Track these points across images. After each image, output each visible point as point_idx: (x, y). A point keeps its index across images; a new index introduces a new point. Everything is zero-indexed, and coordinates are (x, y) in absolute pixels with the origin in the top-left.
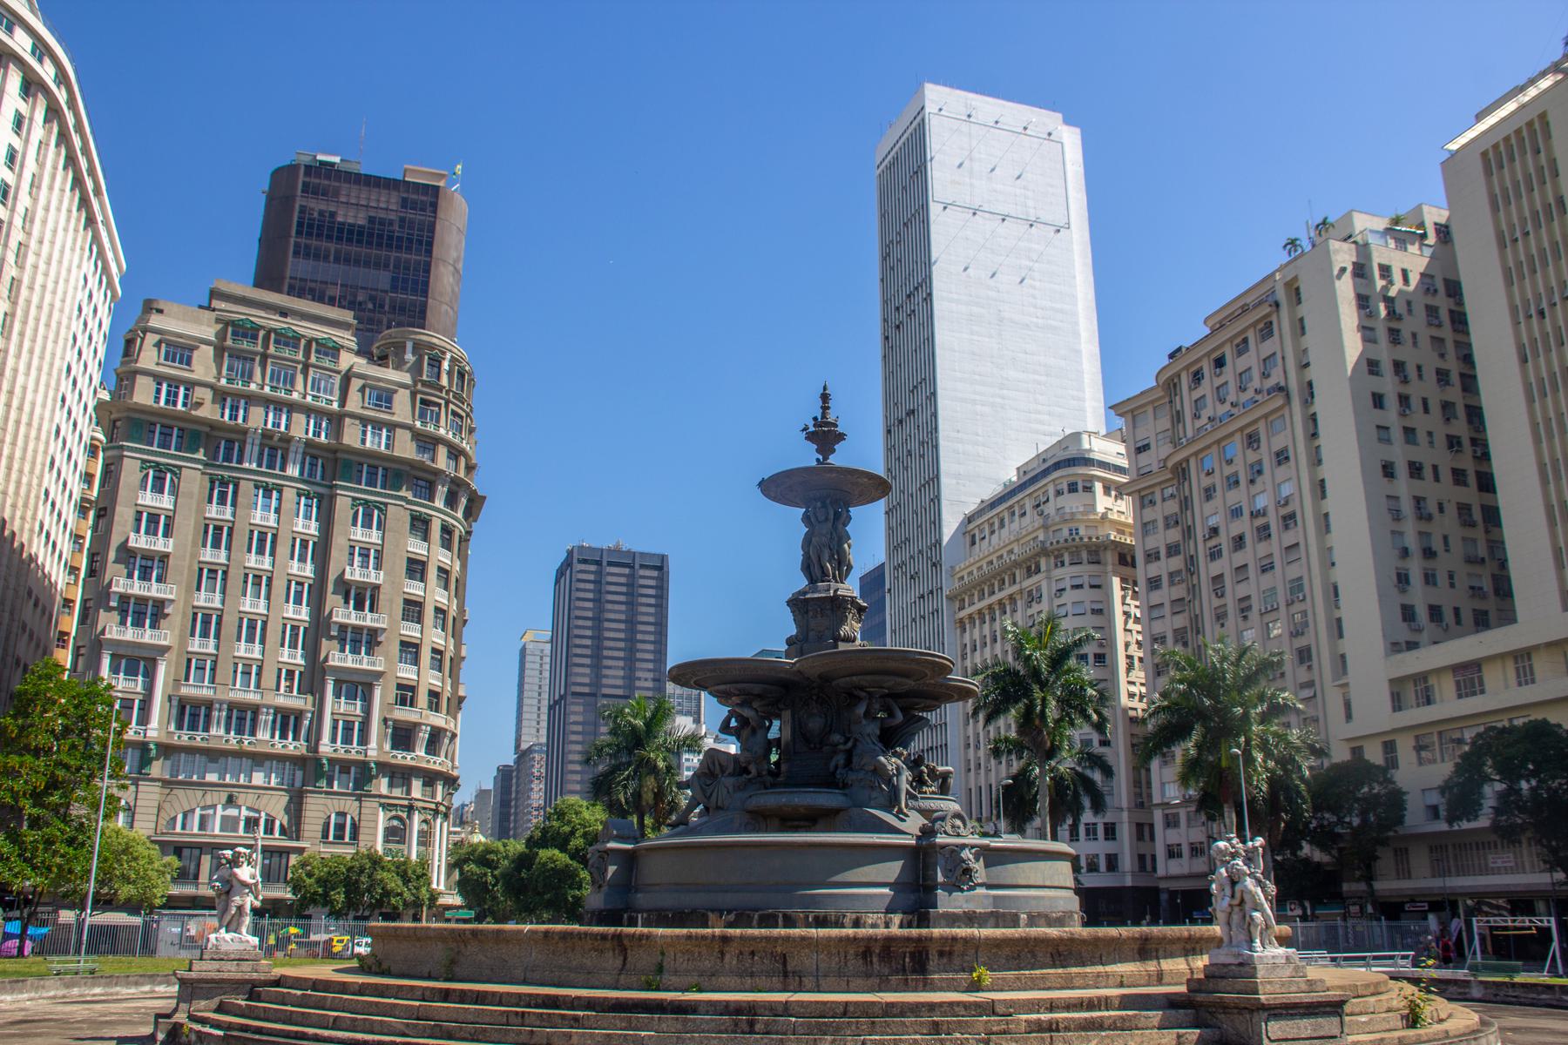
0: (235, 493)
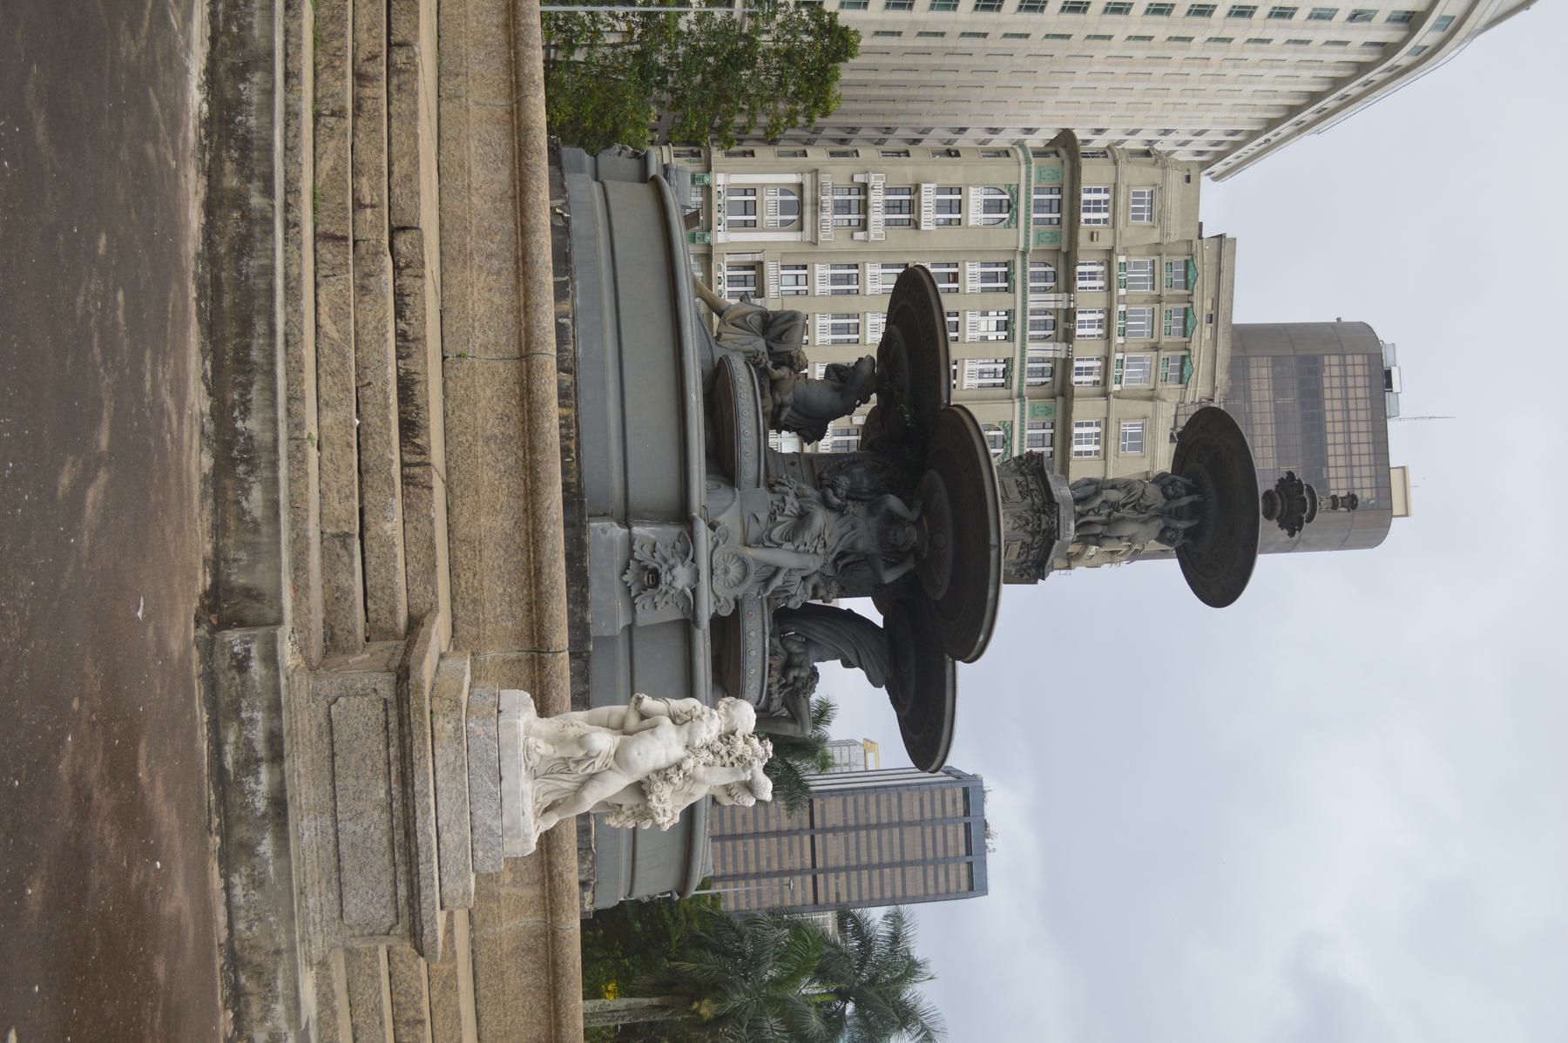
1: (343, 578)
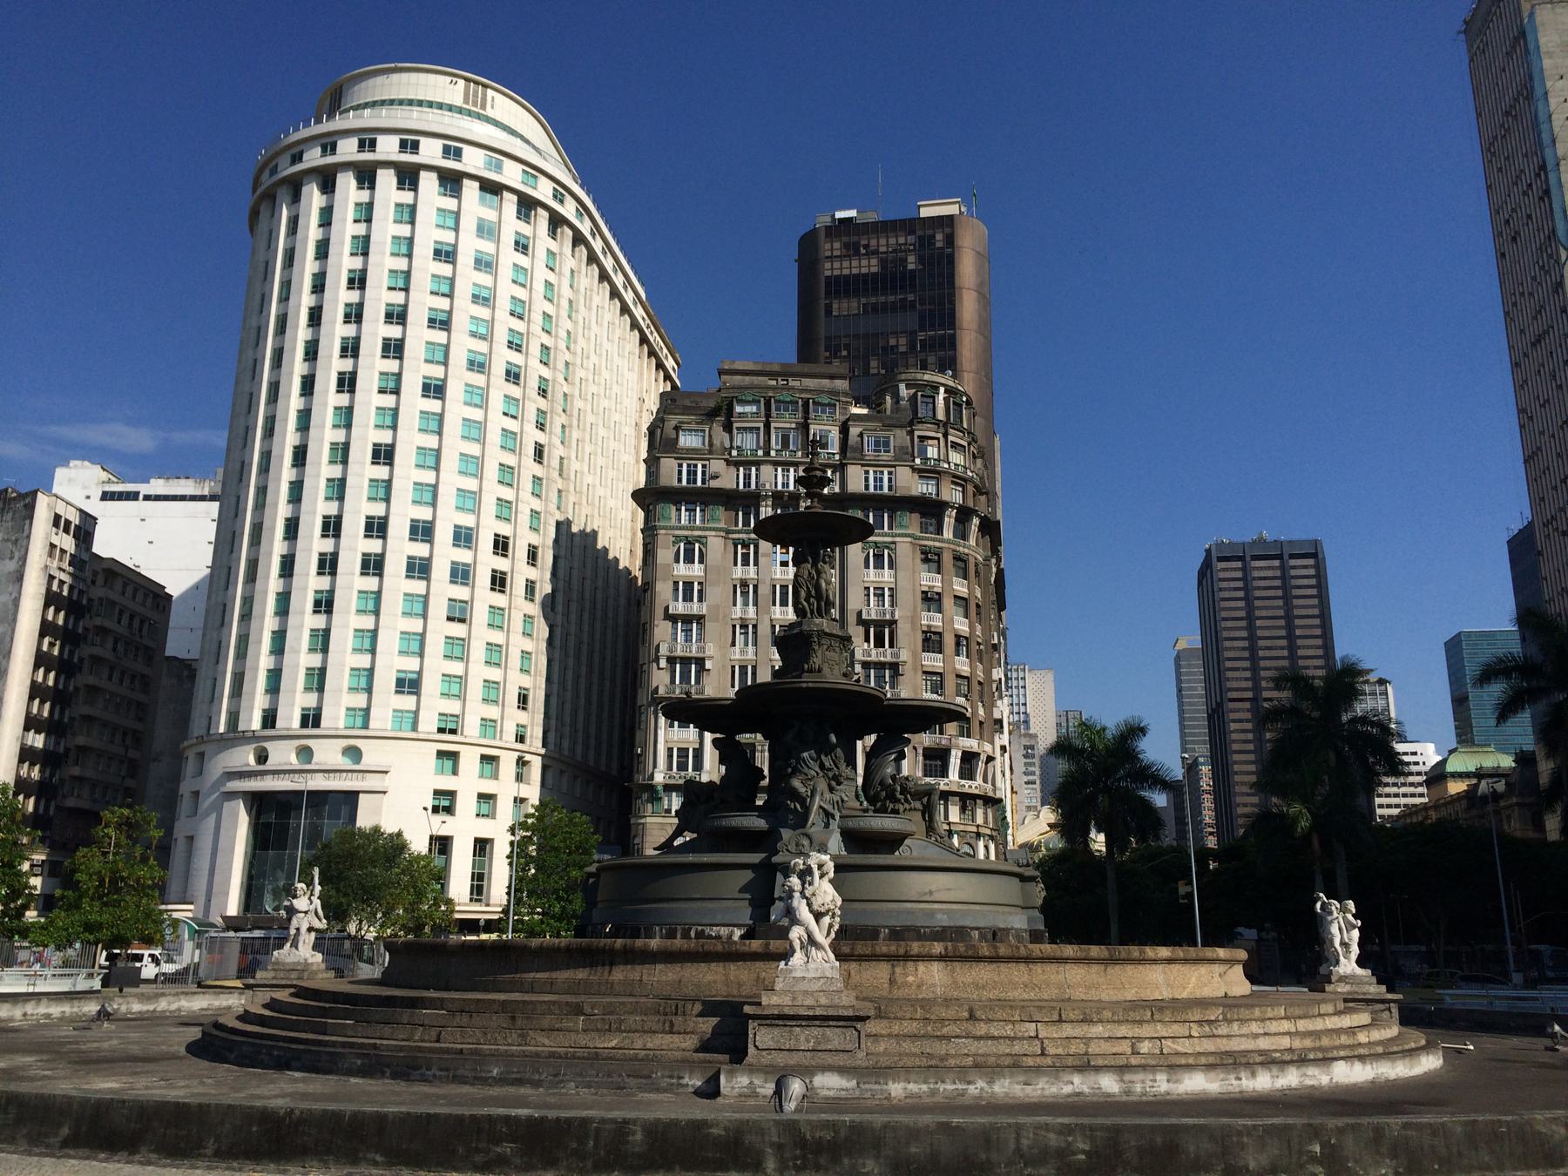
0: (756, 553)
1: (482, 923)
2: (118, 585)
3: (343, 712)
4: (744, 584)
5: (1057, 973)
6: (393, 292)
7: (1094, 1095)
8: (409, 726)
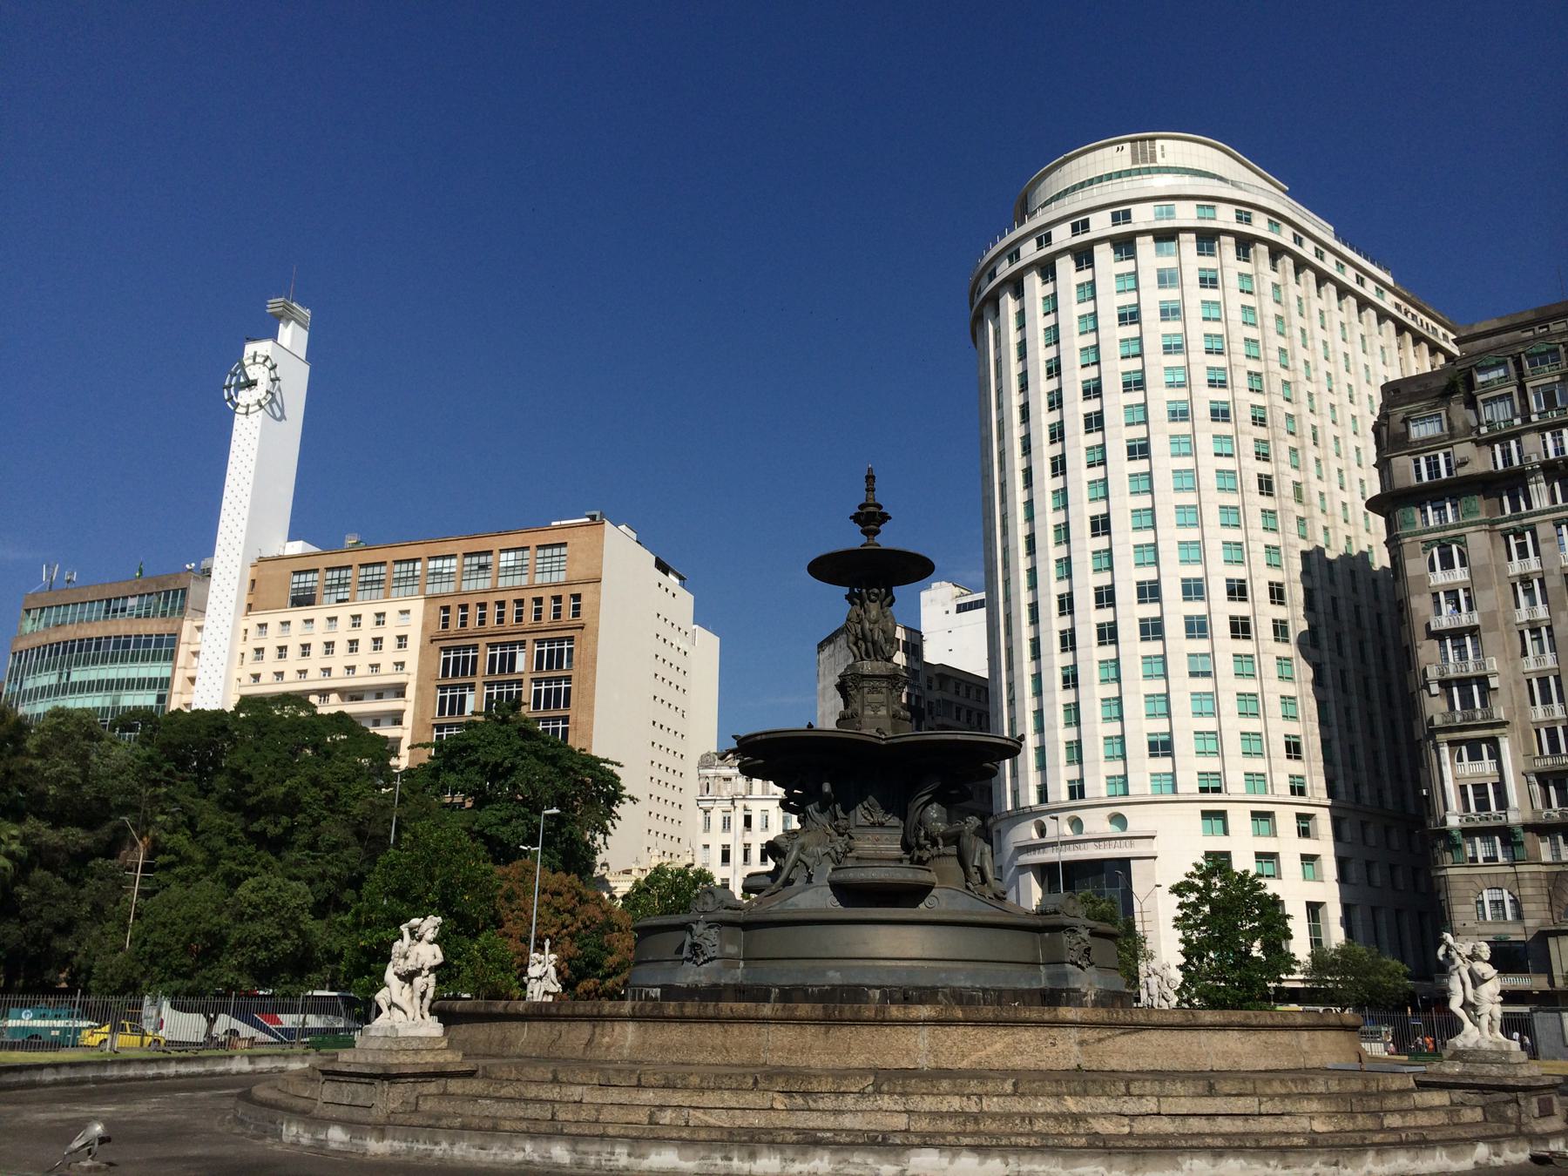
2: (952, 686)
3: (1103, 781)
4: (1526, 580)
5: (758, 1035)
6: (1087, 369)
7: (545, 1164)
8: (1170, 789)
